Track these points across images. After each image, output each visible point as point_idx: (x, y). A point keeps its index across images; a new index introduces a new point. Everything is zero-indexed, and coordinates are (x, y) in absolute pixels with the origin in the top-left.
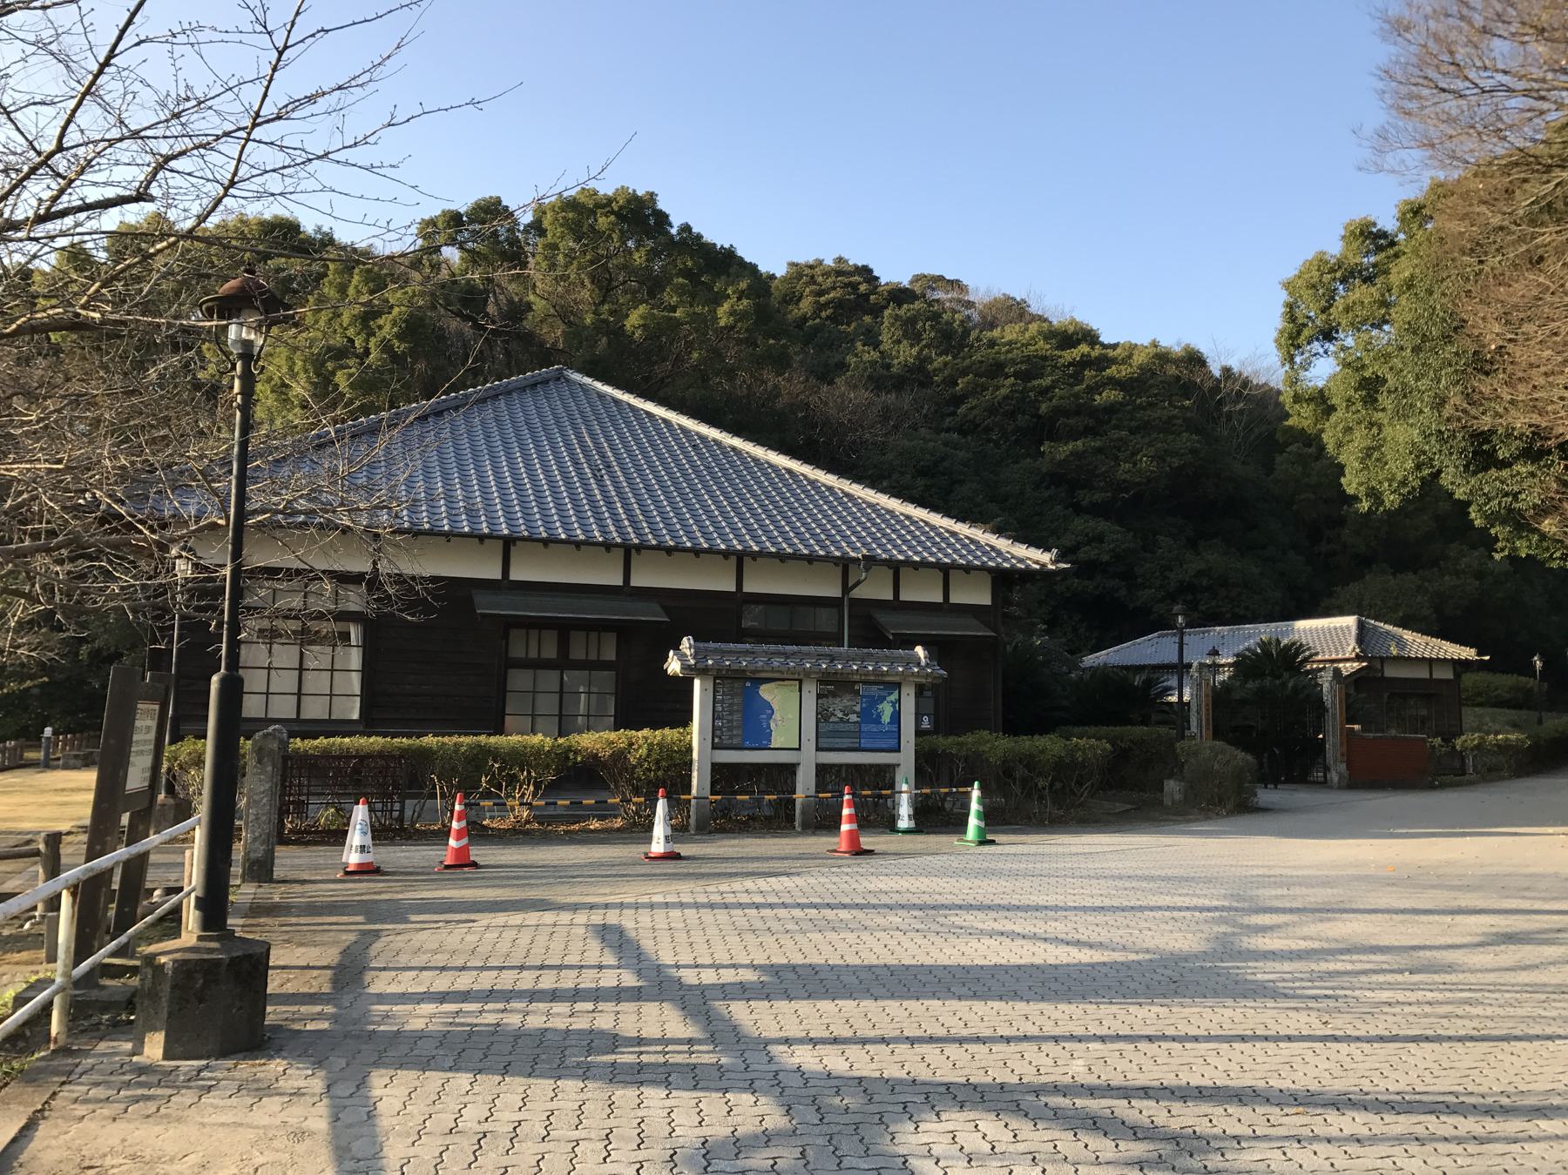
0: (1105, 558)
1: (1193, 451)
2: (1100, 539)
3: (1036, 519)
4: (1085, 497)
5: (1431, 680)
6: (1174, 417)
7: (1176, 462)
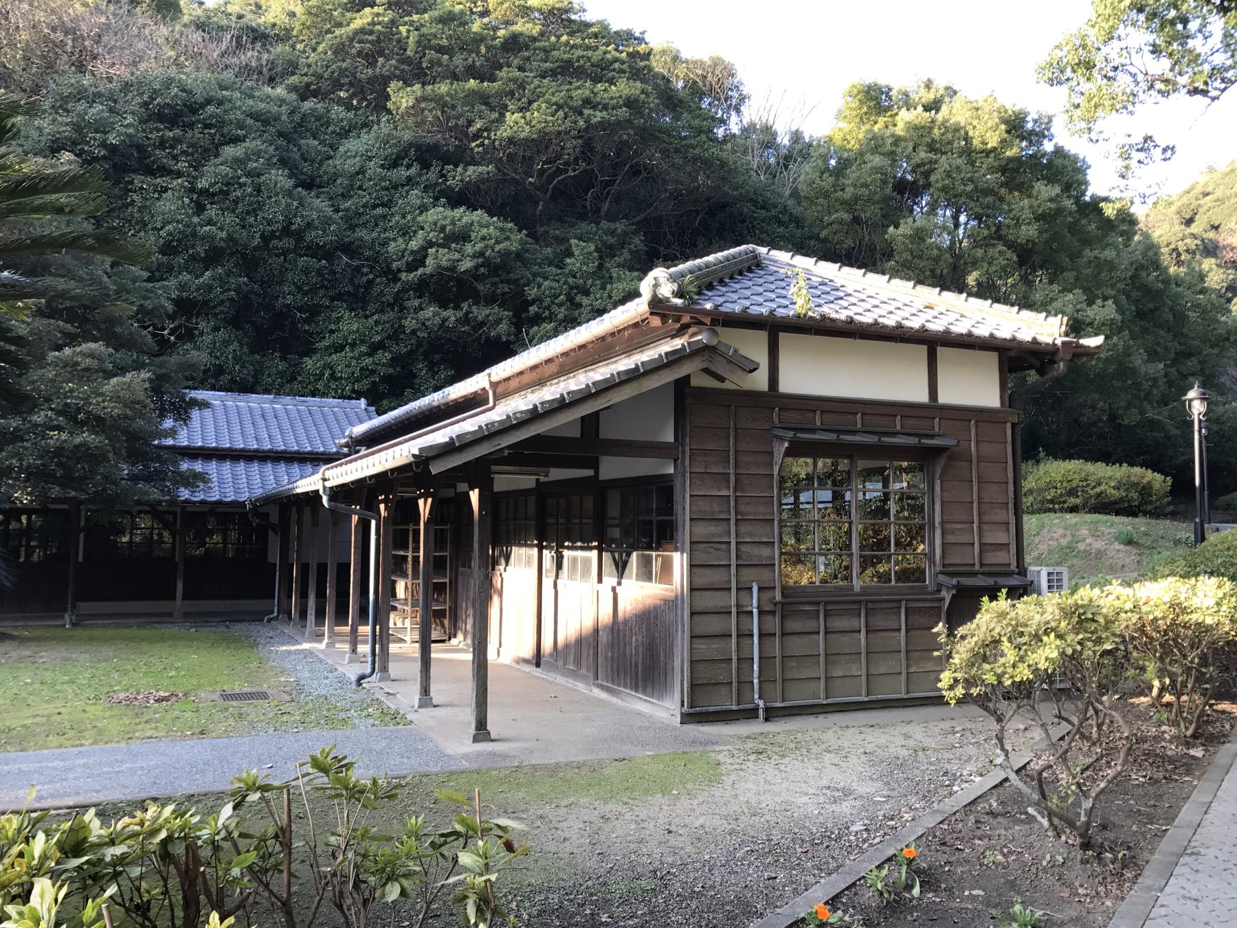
0: (467, 264)
1: (630, 103)
2: (463, 236)
3: (379, 211)
4: (461, 175)
5: (933, 410)
6: (616, 60)
7: (598, 116)
